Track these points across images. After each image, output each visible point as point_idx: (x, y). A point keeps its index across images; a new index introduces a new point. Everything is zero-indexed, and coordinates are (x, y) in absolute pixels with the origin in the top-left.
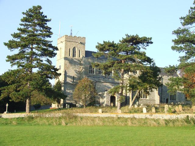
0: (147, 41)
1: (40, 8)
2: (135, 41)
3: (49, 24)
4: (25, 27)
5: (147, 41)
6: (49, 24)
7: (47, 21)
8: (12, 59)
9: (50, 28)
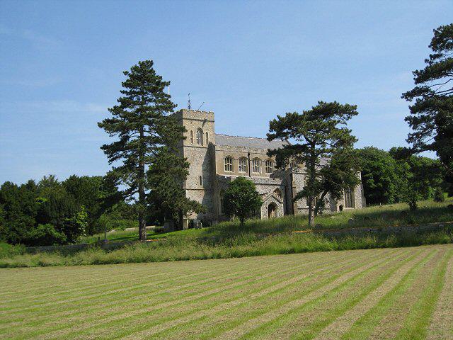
0: (350, 111)
1: (152, 63)
2: (327, 110)
3: (167, 90)
4: (128, 96)
5: (350, 111)
6: (167, 90)
7: (45, 179)
8: (111, 150)
9: (170, 96)
